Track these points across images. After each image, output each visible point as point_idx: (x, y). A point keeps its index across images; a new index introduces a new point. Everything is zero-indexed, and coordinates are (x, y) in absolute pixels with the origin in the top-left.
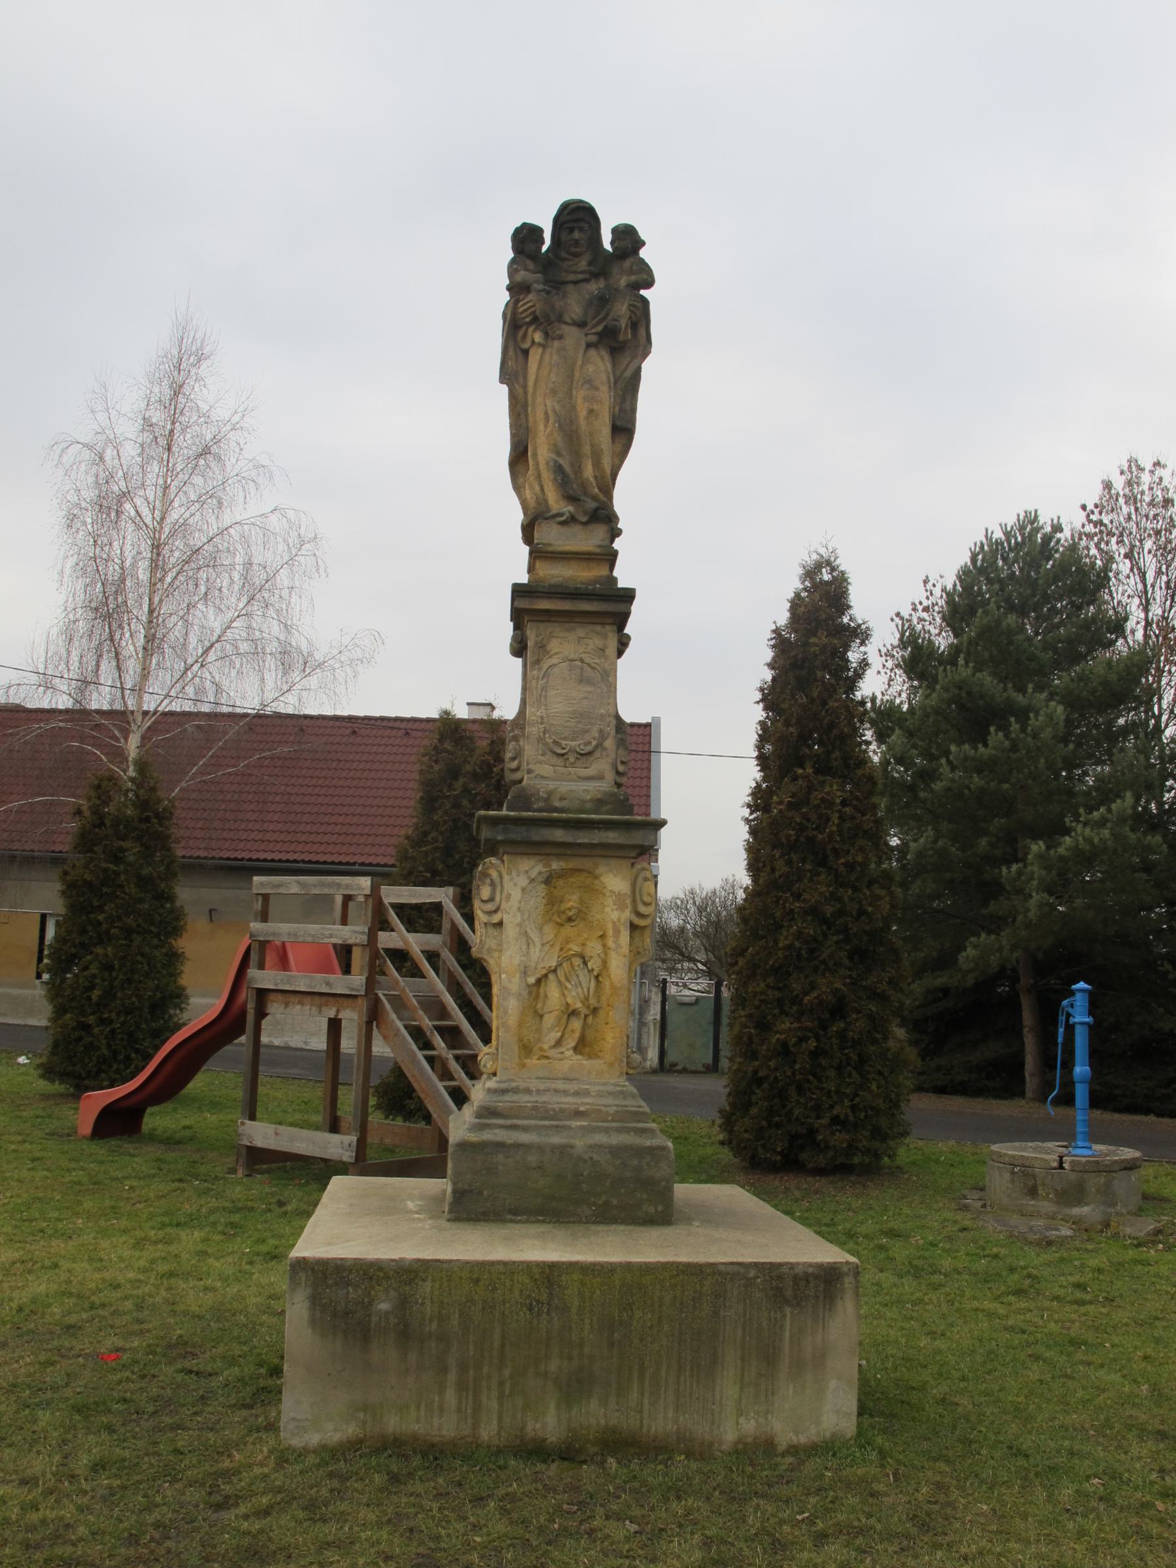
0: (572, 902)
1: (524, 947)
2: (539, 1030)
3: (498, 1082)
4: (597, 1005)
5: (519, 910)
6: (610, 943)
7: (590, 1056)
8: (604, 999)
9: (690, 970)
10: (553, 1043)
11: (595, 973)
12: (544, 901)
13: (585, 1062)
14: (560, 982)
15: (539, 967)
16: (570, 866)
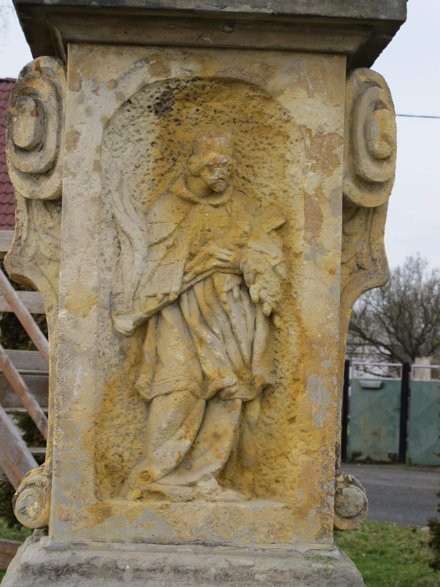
0: (215, 149)
1: (109, 252)
2: (142, 433)
3: (48, 549)
4: (269, 380)
5: (97, 167)
6: (299, 242)
7: (254, 493)
8: (285, 367)
9: (371, 354)
10: (171, 462)
11: (267, 309)
12: (155, 152)
13: (243, 506)
15: (143, 294)
16: (211, 74)
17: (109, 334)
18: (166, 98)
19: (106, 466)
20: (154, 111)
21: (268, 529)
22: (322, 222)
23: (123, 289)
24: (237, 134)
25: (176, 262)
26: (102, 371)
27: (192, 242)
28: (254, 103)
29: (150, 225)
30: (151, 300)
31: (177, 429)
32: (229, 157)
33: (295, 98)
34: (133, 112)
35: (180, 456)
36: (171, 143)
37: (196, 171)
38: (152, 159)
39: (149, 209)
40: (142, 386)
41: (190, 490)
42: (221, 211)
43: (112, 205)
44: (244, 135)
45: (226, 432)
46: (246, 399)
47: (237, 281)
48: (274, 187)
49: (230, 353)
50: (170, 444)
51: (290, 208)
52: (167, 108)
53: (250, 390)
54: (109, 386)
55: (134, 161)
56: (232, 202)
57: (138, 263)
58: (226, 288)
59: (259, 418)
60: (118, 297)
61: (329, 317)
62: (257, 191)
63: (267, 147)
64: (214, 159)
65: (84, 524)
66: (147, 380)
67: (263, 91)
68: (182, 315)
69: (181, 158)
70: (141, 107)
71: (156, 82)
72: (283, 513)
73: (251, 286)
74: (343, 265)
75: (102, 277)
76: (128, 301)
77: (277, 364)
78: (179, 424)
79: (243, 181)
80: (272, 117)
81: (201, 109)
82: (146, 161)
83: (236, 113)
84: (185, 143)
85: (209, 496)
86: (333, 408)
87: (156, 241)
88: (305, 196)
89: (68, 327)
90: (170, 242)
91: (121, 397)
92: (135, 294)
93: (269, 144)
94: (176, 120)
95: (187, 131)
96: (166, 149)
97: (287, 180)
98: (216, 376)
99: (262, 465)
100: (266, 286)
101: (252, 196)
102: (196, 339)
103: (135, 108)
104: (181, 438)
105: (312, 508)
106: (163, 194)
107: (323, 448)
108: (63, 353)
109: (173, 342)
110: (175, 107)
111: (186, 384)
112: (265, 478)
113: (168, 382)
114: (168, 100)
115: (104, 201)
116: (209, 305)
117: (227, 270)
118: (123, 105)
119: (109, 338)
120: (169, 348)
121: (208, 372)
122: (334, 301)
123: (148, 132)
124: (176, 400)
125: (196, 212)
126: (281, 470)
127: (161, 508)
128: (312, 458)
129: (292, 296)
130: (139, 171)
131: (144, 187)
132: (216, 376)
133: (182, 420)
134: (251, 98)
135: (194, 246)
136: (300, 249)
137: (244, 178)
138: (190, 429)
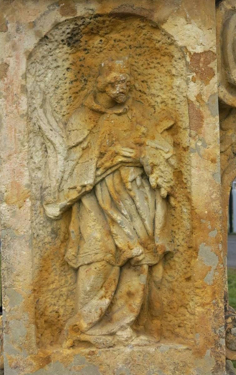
2: (72, 293)
5: (24, 89)
6: (185, 139)
7: (161, 335)
10: (95, 317)
11: (164, 192)
12: (70, 75)
13: (152, 350)
14: (102, 211)
15: (66, 187)
16: (109, 10)
17: (41, 219)
18: (75, 33)
19: (45, 321)
20: (66, 44)
21: (174, 367)
22: (203, 122)
23: (50, 184)
24: (133, 57)
25: (90, 161)
26: (37, 249)
27: (101, 144)
28: (144, 31)
29: (68, 132)
30: (72, 191)
31: (98, 291)
32: (127, 75)
33: (176, 25)
34: (50, 45)
35: (102, 312)
36: (82, 68)
37: (102, 88)
38: (68, 81)
39: (68, 120)
40: (70, 258)
41: (110, 338)
42: (124, 117)
43: (38, 119)
44: (139, 57)
45: (137, 291)
46: (151, 264)
47: (139, 172)
48: (164, 96)
49: (136, 229)
50: (94, 302)
51: (178, 112)
52: (77, 41)
53: (155, 256)
54: (45, 260)
55: (54, 83)
56: (132, 110)
57: (61, 163)
58: (130, 178)
59: (163, 277)
60: (47, 190)
61: (213, 197)
62: (151, 101)
63: (156, 65)
64: (114, 77)
65: (29, 369)
66: (73, 253)
67: (151, 21)
68: (98, 201)
69: (91, 79)
70: (56, 41)
71: (66, 21)
72: (185, 353)
73: (150, 176)
74: (222, 154)
75: (33, 176)
76: (54, 193)
77: (174, 235)
78: (100, 287)
79: (140, 93)
80: (159, 41)
81: (103, 39)
82: (64, 83)
83: (131, 41)
84: (93, 67)
85: (126, 343)
86: (220, 269)
87: (74, 145)
88: (188, 101)
89: (8, 217)
90: (85, 145)
91: (54, 267)
92: (59, 187)
93: (158, 63)
94: (85, 50)
95: (94, 57)
96: (79, 72)
97: (174, 90)
98: (126, 248)
99: (167, 314)
100: (162, 175)
101: (147, 104)
102: (109, 220)
103: (52, 42)
104: (102, 297)
105: (208, 348)
106: (78, 108)
107: (214, 301)
108: (6, 238)
109: (92, 224)
110: (84, 38)
111: (103, 256)
112: (171, 323)
113: (89, 255)
114: (77, 34)
115: (31, 117)
116: (117, 192)
117: (130, 164)
118: (41, 40)
119: (42, 222)
120: (88, 228)
121: (119, 245)
122: (216, 184)
123: (63, 60)
124: (96, 268)
125: (103, 121)
126: (182, 318)
127: (89, 354)
128: (205, 309)
129: (183, 181)
130: (59, 91)
131: (64, 103)
132: (126, 248)
133: (102, 283)
134: (142, 28)
135: (103, 147)
136: (187, 145)
137: (140, 91)
138: (108, 290)
